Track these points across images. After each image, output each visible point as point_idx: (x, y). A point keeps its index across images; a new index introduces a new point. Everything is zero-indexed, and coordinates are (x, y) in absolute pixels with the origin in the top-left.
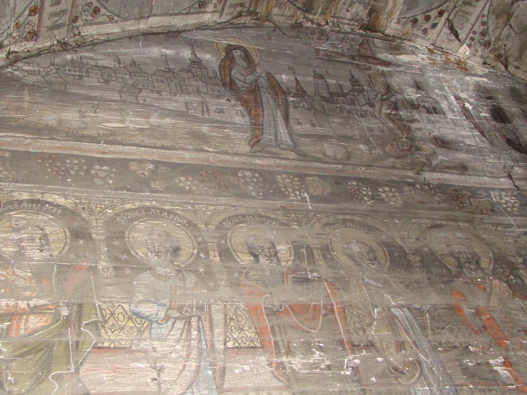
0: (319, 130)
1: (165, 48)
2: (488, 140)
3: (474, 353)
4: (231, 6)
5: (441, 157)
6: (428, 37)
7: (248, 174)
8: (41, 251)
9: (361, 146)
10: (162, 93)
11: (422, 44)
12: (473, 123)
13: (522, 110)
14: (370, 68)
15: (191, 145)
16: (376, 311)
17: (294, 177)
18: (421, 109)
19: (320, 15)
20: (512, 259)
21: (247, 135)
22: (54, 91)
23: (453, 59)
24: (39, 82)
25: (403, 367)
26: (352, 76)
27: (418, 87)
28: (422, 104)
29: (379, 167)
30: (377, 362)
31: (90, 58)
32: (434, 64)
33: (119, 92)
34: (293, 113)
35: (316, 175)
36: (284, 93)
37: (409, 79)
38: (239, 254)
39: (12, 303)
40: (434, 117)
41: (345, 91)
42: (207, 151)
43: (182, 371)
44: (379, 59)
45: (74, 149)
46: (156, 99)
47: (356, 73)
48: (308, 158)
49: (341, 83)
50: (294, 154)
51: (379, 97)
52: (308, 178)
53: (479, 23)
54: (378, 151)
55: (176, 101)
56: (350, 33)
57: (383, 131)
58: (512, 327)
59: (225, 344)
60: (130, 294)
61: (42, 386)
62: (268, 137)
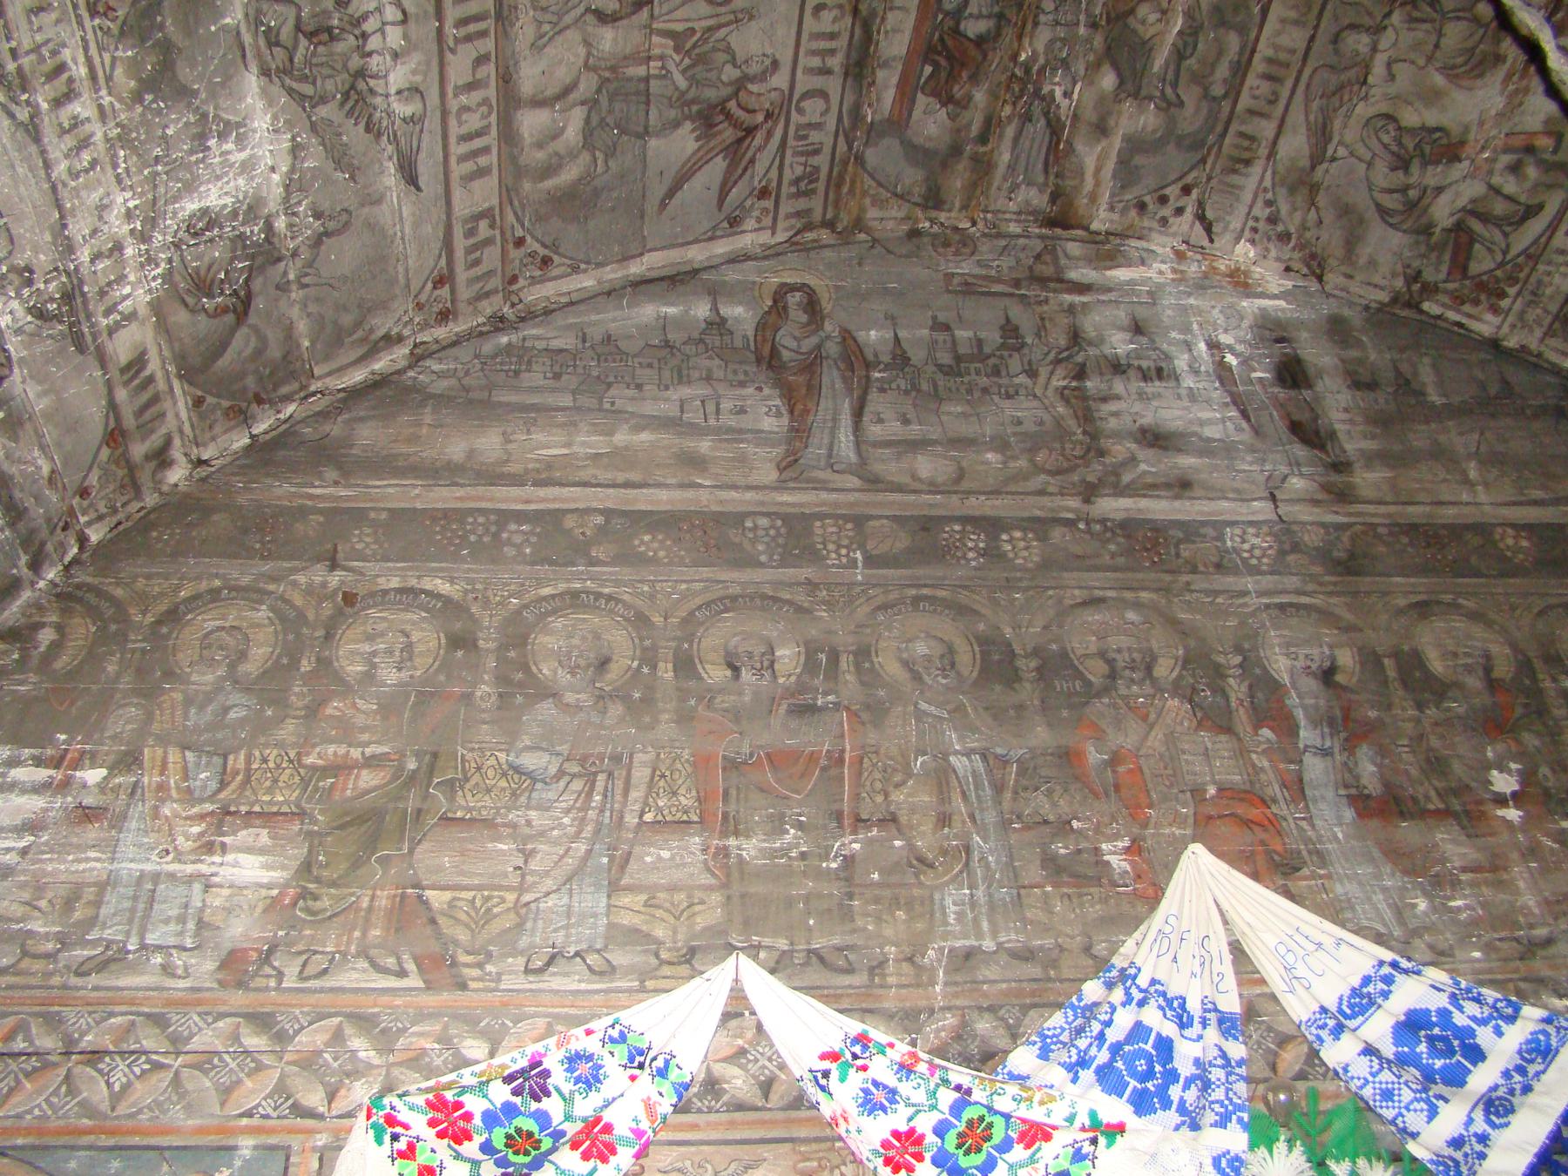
0: (915, 430)
1: (666, 304)
2: (1252, 426)
3: (1079, 832)
4: (788, 216)
5: (1143, 467)
6: (1171, 230)
7: (763, 522)
8: (400, 669)
9: (989, 456)
10: (647, 387)
11: (1162, 245)
12: (1231, 394)
13: (1343, 361)
14: (1046, 301)
15: (675, 476)
16: (920, 759)
17: (847, 522)
18: (1131, 373)
19: (960, 210)
20: (1221, 659)
21: (778, 451)
22: (471, 402)
23: (1223, 268)
24: (451, 389)
25: (936, 858)
26: (1008, 320)
27: (1137, 329)
28: (1136, 363)
29: (1013, 493)
30: (893, 847)
31: (538, 338)
32: (1181, 280)
33: (574, 393)
34: (876, 403)
35: (887, 517)
36: (868, 366)
37: (1123, 314)
38: (708, 666)
39: (342, 750)
40: (1155, 387)
41: (987, 350)
42: (701, 486)
43: (562, 857)
44: (1069, 282)
45: (481, 499)
46: (633, 399)
47: (1017, 313)
48: (880, 486)
49: (983, 335)
50: (856, 480)
51: (1052, 356)
52: (871, 523)
53: (1260, 203)
54: (1022, 463)
55: (666, 400)
56: (1019, 236)
57: (1041, 423)
58: (1172, 785)
59: (641, 817)
60: (512, 735)
61: (359, 872)
62: (815, 450)
